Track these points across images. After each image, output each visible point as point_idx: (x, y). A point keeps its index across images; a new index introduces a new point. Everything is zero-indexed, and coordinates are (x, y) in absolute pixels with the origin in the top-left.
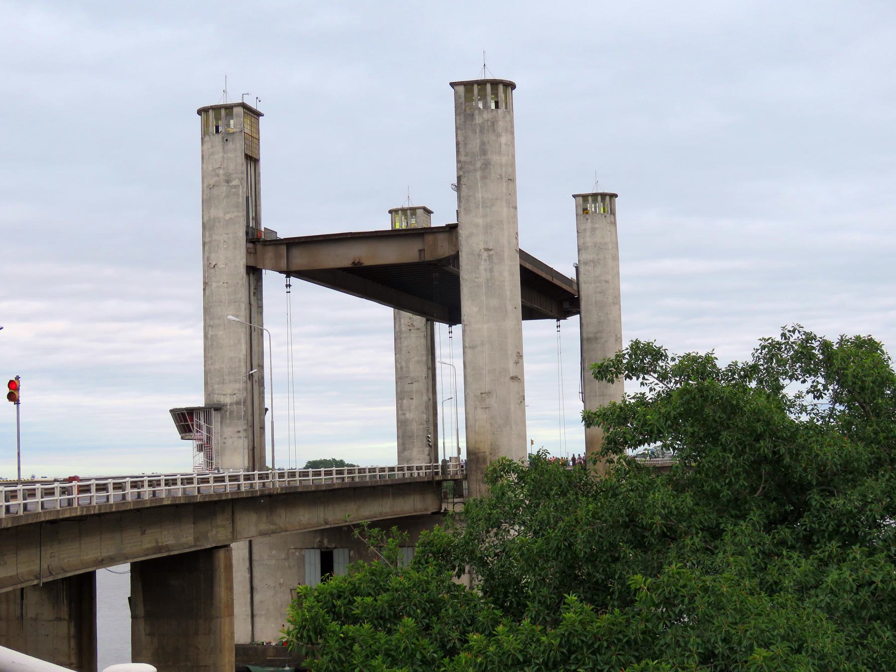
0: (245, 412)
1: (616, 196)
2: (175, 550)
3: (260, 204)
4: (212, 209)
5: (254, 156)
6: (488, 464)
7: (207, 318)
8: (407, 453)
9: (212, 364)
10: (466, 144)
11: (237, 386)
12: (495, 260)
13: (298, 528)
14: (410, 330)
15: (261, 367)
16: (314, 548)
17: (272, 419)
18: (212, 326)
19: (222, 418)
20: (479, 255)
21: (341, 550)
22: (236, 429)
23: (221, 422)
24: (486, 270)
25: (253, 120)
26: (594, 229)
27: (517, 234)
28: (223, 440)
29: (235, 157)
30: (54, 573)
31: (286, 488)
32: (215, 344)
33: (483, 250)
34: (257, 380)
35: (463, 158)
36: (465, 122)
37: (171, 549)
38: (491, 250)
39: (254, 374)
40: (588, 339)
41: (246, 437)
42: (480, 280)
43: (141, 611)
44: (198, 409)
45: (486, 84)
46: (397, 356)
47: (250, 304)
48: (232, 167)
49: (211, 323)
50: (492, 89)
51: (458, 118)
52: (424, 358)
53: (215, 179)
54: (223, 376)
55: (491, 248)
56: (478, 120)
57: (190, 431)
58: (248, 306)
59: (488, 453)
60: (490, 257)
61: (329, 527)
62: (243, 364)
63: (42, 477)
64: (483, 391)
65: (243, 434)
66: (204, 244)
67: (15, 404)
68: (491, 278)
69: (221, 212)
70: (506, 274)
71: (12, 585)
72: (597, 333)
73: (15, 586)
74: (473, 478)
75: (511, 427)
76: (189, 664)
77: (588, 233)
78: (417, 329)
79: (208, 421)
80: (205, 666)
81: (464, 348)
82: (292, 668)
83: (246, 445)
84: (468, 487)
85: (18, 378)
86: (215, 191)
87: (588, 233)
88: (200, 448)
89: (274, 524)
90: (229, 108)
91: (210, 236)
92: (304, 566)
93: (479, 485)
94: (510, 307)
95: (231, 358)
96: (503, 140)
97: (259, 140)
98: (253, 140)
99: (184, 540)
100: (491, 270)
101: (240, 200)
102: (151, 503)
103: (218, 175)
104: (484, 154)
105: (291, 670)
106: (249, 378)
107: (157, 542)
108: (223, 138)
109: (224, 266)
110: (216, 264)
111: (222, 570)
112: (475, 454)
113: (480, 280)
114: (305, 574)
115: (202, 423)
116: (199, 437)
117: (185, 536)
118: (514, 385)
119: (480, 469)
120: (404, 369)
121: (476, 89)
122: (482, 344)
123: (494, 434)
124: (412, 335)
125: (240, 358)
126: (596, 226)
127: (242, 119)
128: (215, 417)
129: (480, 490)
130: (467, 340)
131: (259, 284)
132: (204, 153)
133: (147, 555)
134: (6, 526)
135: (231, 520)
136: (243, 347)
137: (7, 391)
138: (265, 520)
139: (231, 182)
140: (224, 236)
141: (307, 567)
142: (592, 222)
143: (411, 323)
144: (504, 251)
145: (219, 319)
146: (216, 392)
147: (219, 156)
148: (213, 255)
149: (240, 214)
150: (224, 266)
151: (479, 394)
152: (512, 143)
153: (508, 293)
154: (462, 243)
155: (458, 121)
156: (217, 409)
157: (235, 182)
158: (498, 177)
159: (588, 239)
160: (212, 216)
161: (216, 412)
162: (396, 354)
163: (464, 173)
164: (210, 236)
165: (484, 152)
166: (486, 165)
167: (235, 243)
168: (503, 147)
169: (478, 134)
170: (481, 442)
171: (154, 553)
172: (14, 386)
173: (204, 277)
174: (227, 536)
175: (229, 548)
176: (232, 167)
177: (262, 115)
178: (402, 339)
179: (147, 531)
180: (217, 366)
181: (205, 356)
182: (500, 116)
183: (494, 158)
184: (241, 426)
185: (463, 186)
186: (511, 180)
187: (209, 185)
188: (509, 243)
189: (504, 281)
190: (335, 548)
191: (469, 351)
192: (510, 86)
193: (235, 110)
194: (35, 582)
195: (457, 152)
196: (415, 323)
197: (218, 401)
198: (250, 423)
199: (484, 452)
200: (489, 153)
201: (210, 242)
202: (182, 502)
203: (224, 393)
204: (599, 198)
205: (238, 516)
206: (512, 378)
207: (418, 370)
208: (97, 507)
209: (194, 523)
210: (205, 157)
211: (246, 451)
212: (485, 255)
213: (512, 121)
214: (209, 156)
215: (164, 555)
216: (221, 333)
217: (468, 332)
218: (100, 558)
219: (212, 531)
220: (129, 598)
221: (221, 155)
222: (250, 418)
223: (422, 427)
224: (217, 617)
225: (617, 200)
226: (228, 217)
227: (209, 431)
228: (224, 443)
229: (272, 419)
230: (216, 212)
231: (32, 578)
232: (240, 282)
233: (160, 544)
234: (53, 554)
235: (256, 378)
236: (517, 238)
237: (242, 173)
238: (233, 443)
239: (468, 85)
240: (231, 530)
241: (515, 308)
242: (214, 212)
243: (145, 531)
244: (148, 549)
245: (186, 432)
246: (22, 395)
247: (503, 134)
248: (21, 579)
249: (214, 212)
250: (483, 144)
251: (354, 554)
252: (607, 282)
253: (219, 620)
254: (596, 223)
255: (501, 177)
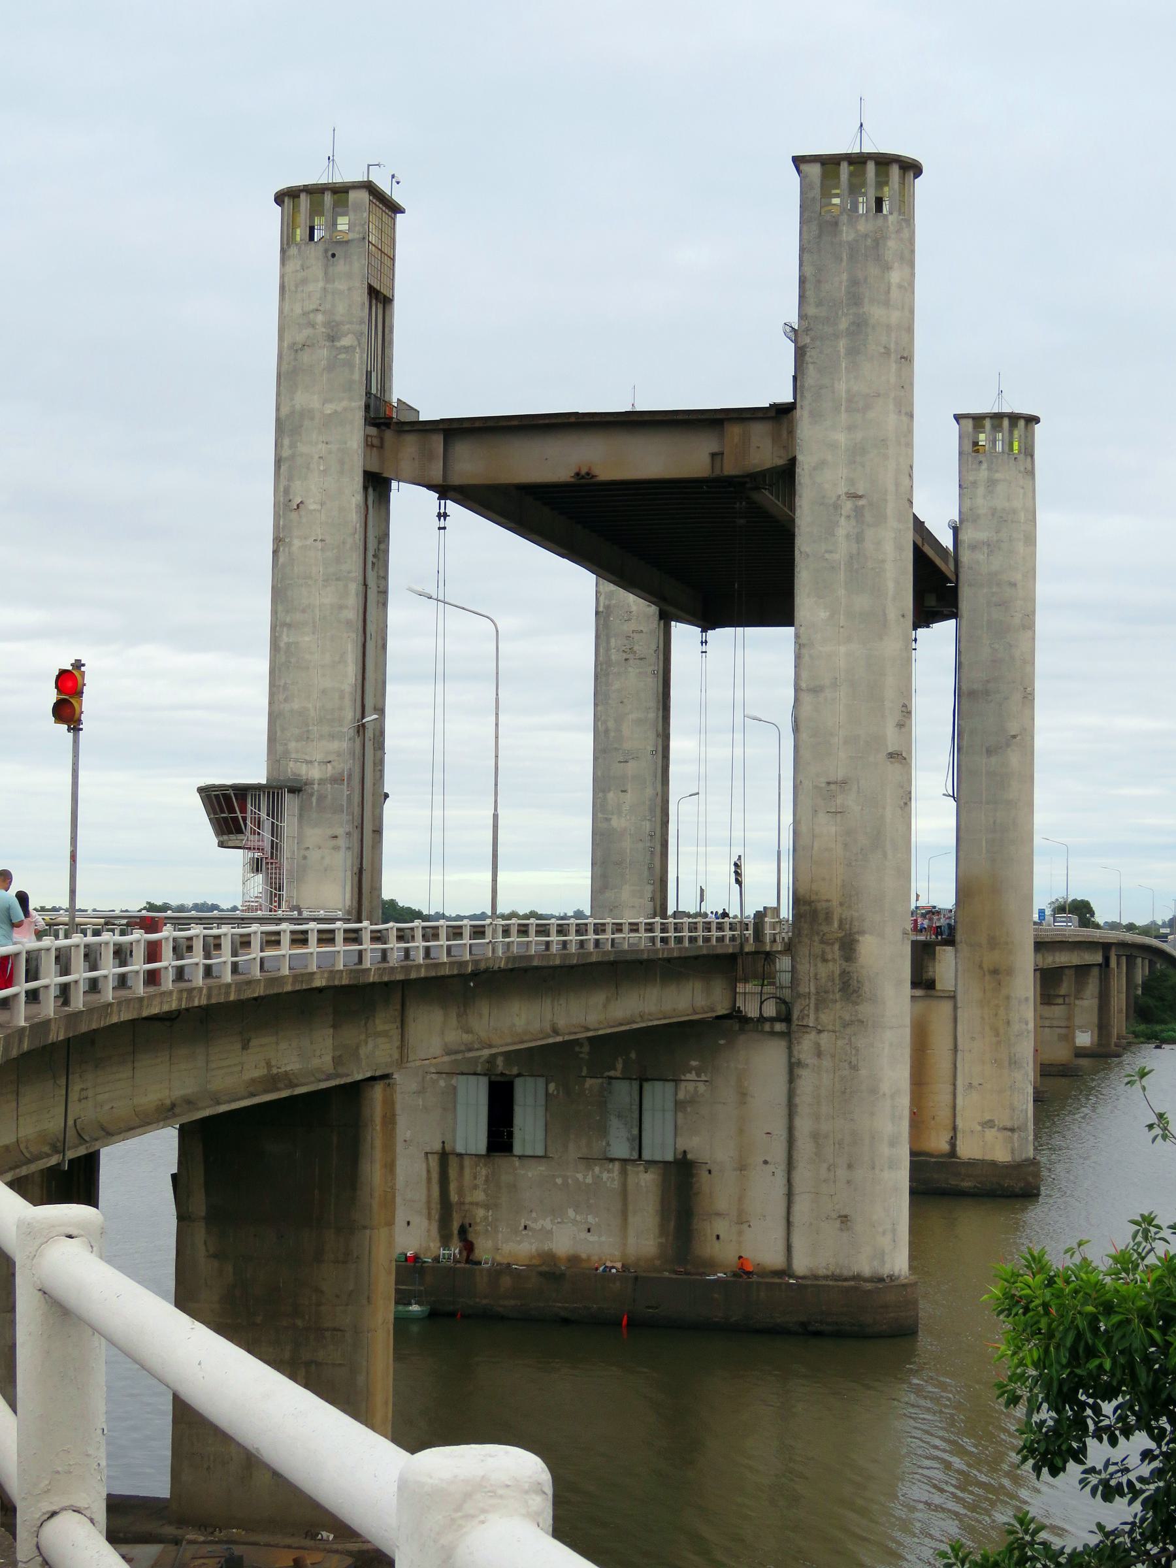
0: (349, 797)
1: (1036, 420)
2: (303, 1085)
3: (391, 388)
4: (299, 393)
5: (385, 291)
6: (836, 925)
7: (280, 608)
8: (609, 895)
9: (286, 700)
10: (819, 281)
11: (335, 745)
12: (868, 517)
13: (509, 1041)
14: (626, 660)
15: (381, 710)
16: (475, 1074)
17: (496, 809)
18: (289, 626)
19: (301, 809)
20: (837, 507)
21: (529, 1079)
22: (330, 832)
23: (301, 816)
24: (848, 536)
25: (385, 218)
26: (991, 483)
27: (911, 467)
28: (302, 852)
29: (349, 289)
30: (87, 1138)
31: (515, 958)
32: (293, 660)
33: (844, 497)
34: (372, 736)
35: (811, 311)
36: (820, 236)
37: (295, 1081)
38: (861, 497)
39: (366, 724)
40: (972, 694)
41: (349, 848)
42: (837, 556)
43: (199, 1205)
44: (257, 788)
45: (865, 163)
46: (599, 708)
47: (365, 585)
48: (341, 309)
49: (288, 620)
50: (877, 174)
51: (805, 228)
52: (652, 715)
53: (308, 332)
54: (307, 725)
55: (860, 493)
56: (847, 234)
57: (239, 831)
58: (361, 588)
59: (835, 903)
60: (858, 512)
61: (559, 1039)
62: (348, 703)
63: (122, 911)
64: (831, 780)
65: (341, 842)
66: (278, 462)
67: (69, 730)
68: (858, 554)
69: (316, 397)
70: (889, 548)
71: (11, 1169)
72: (988, 681)
73: (18, 1170)
74: (803, 951)
75: (885, 855)
76: (299, 1323)
77: (981, 491)
78: (641, 659)
79: (275, 812)
80: (335, 1329)
81: (796, 691)
82: (424, 1308)
83: (349, 863)
84: (793, 967)
85: (78, 665)
86: (306, 357)
87: (981, 491)
88: (257, 866)
89: (468, 1031)
90: (340, 191)
91: (293, 445)
92: (455, 1107)
93: (816, 965)
94: (892, 614)
95: (324, 692)
96: (895, 277)
97: (393, 259)
98: (384, 257)
99: (316, 1062)
100: (859, 538)
101: (356, 376)
102: (293, 983)
103: (313, 325)
104: (855, 304)
105: (422, 1311)
106: (358, 732)
107: (269, 1065)
108: (326, 251)
109: (318, 507)
110: (301, 502)
111: (378, 1128)
112: (809, 903)
113: (837, 556)
114: (455, 1123)
115: (264, 815)
116: (256, 844)
117: (318, 1053)
118: (893, 770)
119: (818, 934)
120: (612, 734)
121: (846, 171)
122: (835, 685)
123: (849, 865)
124: (630, 669)
125: (343, 691)
126: (998, 476)
127: (365, 215)
128: (290, 803)
129: (816, 975)
130: (804, 675)
131: (382, 546)
132: (286, 279)
133: (253, 1095)
134: (55, 1040)
135: (399, 1020)
136: (351, 670)
137: (52, 696)
138: (453, 1021)
139: (339, 339)
140: (322, 447)
141: (460, 1109)
142: (989, 469)
143: (628, 647)
144: (886, 500)
145: (304, 611)
146: (293, 756)
147: (316, 287)
148: (297, 485)
149: (354, 404)
150: (318, 507)
151: (823, 785)
152: (909, 286)
153: (891, 585)
154: (802, 481)
155: (805, 236)
156: (292, 791)
157: (346, 341)
158: (883, 350)
159: (980, 501)
160: (298, 407)
161: (291, 795)
162: (596, 705)
163: (812, 339)
164: (293, 445)
165: (855, 299)
166: (860, 326)
167: (342, 462)
168: (895, 293)
169: (844, 263)
170: (824, 879)
171: (266, 1091)
172: (70, 684)
173: (276, 527)
174: (391, 1056)
175: (392, 1081)
176: (341, 309)
177: (402, 211)
178: (611, 677)
179: (253, 1043)
180: (296, 706)
181: (272, 685)
182: (892, 228)
183: (876, 312)
184: (342, 826)
185: (811, 367)
186: (906, 359)
187: (294, 344)
188: (897, 485)
189: (883, 561)
190: (519, 1075)
191: (806, 698)
192: (912, 168)
193: (353, 195)
194: (54, 1160)
195: (800, 297)
196: (636, 648)
197: (294, 774)
198: (357, 822)
199: (828, 901)
200: (866, 300)
201: (292, 457)
202: (343, 983)
203: (308, 758)
204: (1006, 422)
205: (411, 1013)
206: (891, 755)
207: (639, 739)
208: (205, 991)
209: (334, 1027)
210: (287, 289)
211: (349, 873)
212: (848, 506)
213: (912, 241)
214: (296, 287)
215: (284, 1094)
216: (307, 639)
217: (806, 659)
218: (168, 1102)
219: (367, 1043)
220: (174, 1176)
221: (321, 284)
222: (357, 810)
223: (640, 845)
224: (365, 1227)
225: (1037, 428)
226: (329, 409)
227: (275, 831)
228: (305, 858)
229: (496, 809)
230: (305, 399)
231: (46, 1149)
232: (350, 541)
233: (275, 1071)
234: (84, 1094)
235: (369, 733)
236: (911, 476)
237: (362, 322)
238: (323, 858)
239: (830, 163)
240: (398, 1043)
241: (903, 616)
242: (302, 399)
243: (249, 1041)
244: (253, 1081)
245: (230, 832)
246: (90, 704)
247: (896, 265)
248: (24, 1151)
249: (302, 399)
250: (854, 282)
251: (557, 1088)
252: (1013, 585)
253: (368, 1232)
254: (997, 471)
255: (887, 352)
